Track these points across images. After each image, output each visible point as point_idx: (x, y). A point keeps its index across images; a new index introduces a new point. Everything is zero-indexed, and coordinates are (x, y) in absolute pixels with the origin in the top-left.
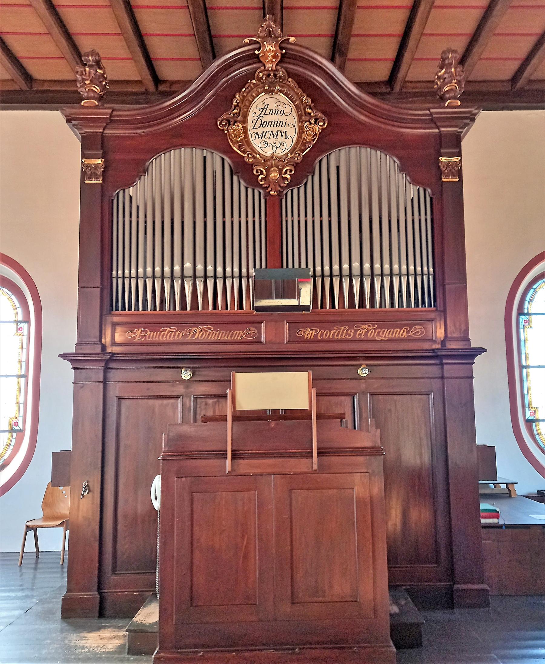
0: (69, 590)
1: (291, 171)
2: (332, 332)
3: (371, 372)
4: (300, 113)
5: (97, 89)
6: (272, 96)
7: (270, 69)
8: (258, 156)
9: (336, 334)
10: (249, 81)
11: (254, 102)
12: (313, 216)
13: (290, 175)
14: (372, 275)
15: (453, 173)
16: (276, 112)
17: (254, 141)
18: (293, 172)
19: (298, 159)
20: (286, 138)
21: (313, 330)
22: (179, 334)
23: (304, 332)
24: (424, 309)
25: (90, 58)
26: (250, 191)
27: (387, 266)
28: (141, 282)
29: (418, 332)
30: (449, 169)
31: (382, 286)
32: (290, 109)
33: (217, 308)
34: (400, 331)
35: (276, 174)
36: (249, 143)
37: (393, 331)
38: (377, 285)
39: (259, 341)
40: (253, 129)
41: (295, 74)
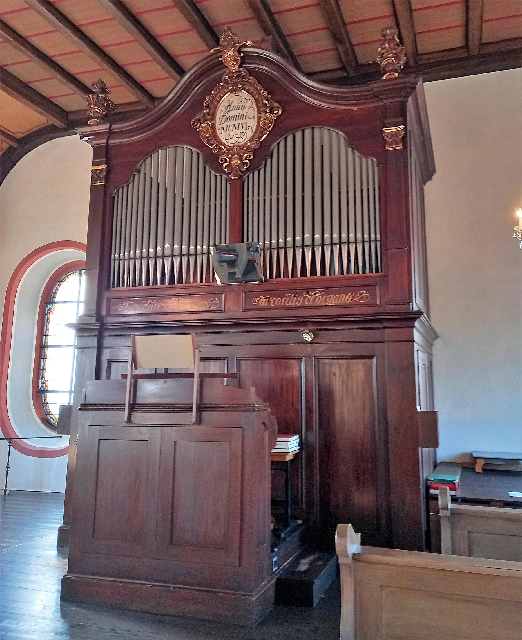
0: (64, 523)
1: (250, 156)
2: (284, 299)
3: (315, 336)
6: (236, 94)
9: (287, 301)
12: (259, 196)
15: (396, 141)
19: (255, 145)
22: (157, 306)
24: (371, 274)
26: (364, 160)
29: (363, 297)
30: (393, 138)
31: (341, 255)
32: (250, 104)
35: (237, 161)
36: (216, 137)
37: (339, 297)
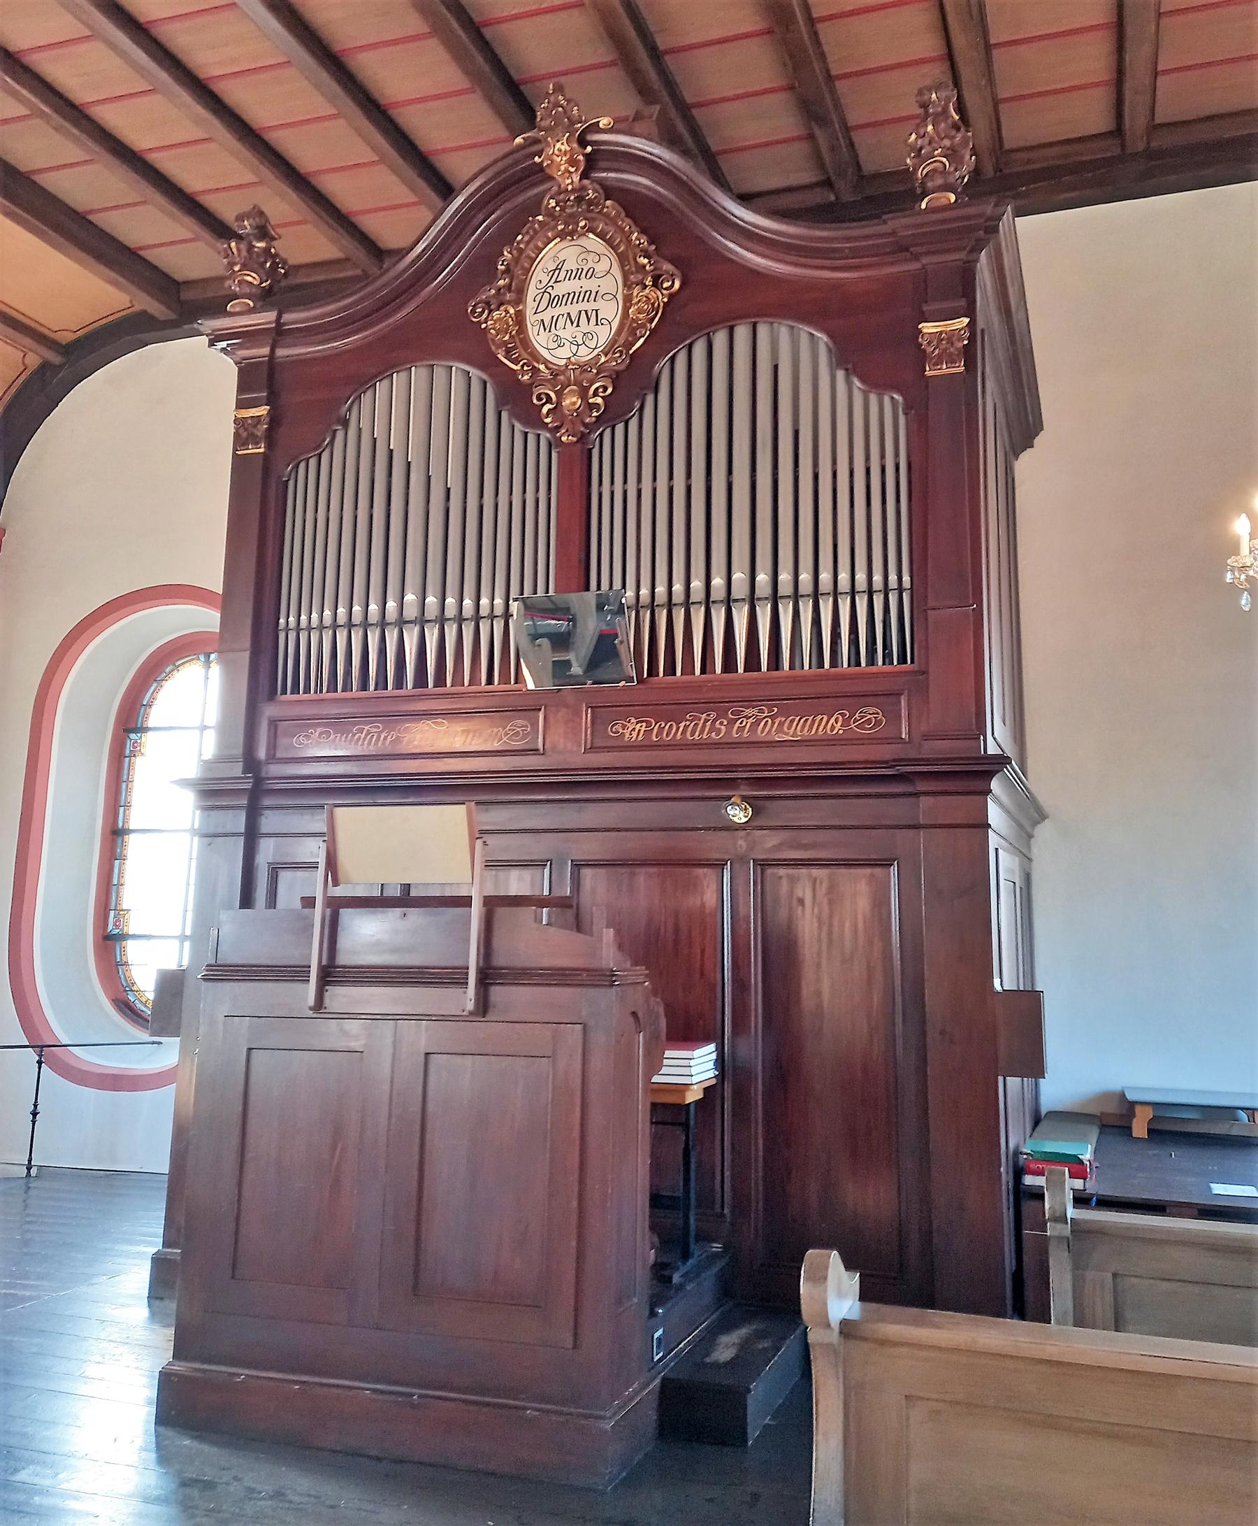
1: (605, 389)
2: (682, 725)
4: (627, 268)
5: (252, 278)
7: (570, 187)
8: (542, 367)
10: (531, 218)
11: (538, 259)
13: (602, 397)
14: (775, 598)
16: (578, 274)
17: (537, 338)
18: (610, 390)
20: (597, 324)
21: (642, 722)
22: (385, 738)
23: (624, 727)
25: (246, 222)
27: (805, 577)
28: (468, 630)
29: (869, 721)
33: (781, 667)
34: (828, 722)
35: (574, 399)
36: (526, 343)
37: (813, 721)
38: (740, 621)
39: (535, 748)
40: (535, 313)
41: (623, 190)
